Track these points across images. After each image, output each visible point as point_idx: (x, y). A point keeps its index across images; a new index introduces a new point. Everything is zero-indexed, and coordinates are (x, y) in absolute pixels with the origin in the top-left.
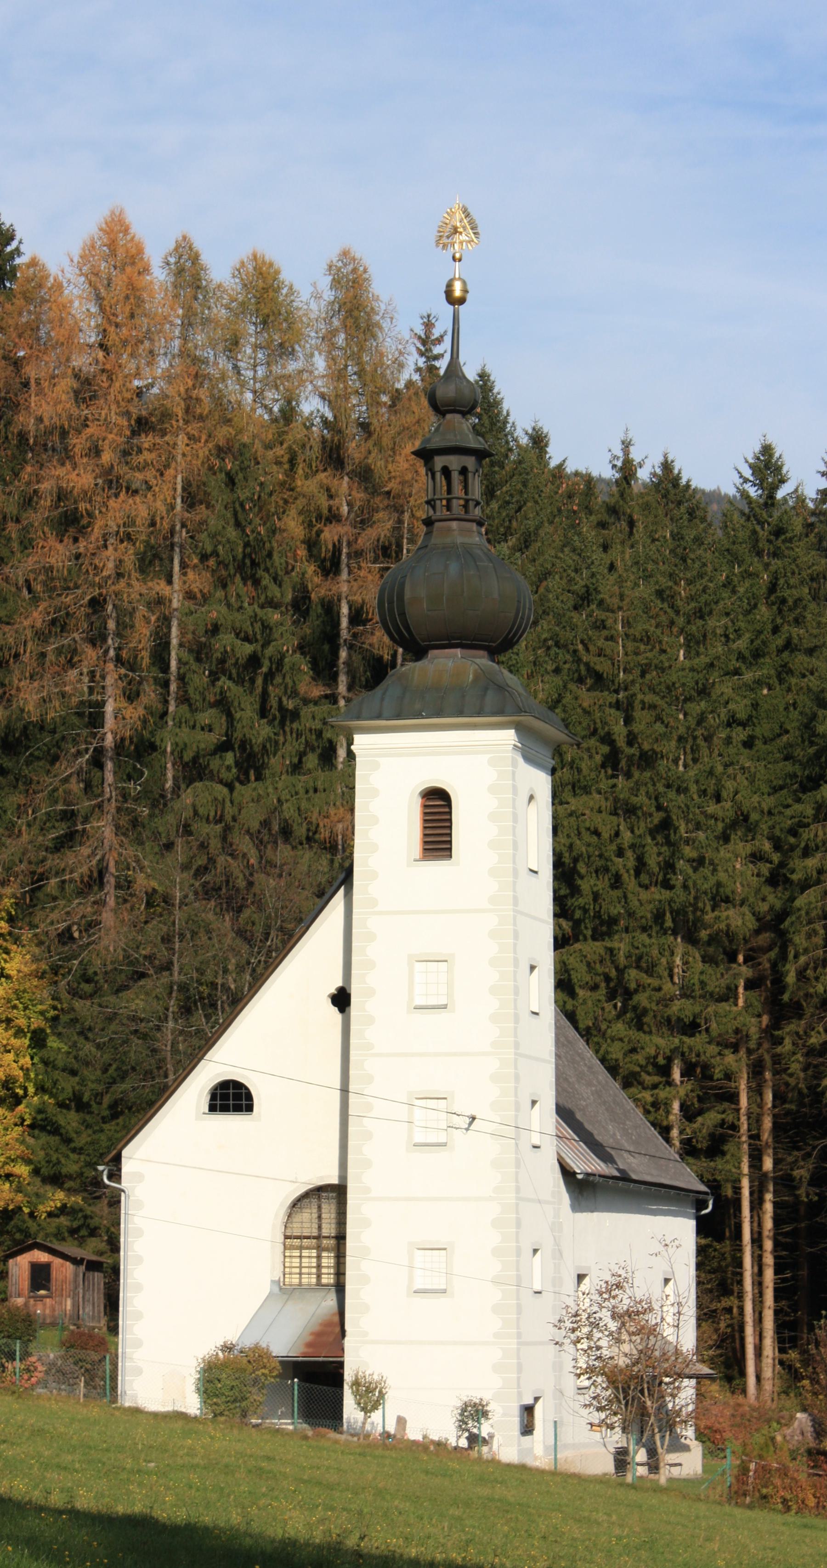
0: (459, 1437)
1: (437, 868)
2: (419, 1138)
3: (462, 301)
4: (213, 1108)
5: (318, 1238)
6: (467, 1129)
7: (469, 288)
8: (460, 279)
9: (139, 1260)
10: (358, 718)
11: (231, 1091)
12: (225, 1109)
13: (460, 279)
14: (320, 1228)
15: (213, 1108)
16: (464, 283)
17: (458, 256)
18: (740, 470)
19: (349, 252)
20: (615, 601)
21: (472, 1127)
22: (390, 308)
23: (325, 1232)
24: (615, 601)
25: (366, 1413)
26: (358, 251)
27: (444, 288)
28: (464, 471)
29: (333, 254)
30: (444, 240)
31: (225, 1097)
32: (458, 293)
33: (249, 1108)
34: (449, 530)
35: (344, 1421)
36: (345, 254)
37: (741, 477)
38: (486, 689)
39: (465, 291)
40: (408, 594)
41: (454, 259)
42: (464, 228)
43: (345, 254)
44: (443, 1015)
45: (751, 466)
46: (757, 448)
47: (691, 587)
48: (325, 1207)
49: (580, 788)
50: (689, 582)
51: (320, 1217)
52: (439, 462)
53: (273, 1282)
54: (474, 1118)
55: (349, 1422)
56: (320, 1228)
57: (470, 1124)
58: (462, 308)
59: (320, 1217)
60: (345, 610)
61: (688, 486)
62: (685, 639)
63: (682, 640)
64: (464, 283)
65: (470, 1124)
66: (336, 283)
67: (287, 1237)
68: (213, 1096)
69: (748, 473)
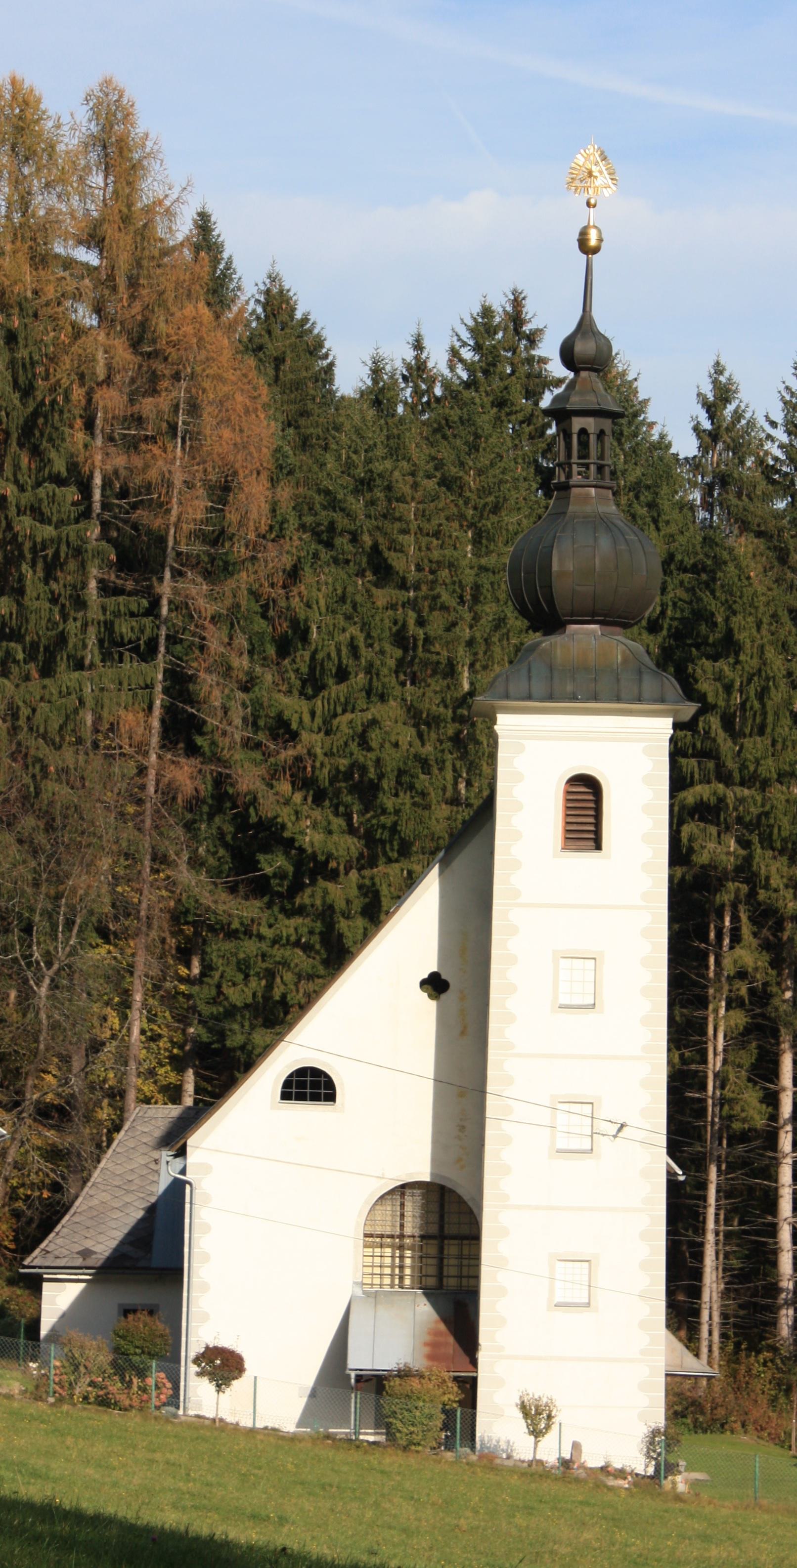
0: (647, 1466)
1: (586, 860)
2: (561, 1144)
3: (596, 250)
4: (286, 1096)
5: (402, 1236)
6: (615, 1136)
7: (604, 236)
8: (595, 227)
9: (206, 1258)
10: (507, 697)
11: (309, 1079)
12: (301, 1097)
13: (595, 227)
14: (402, 1226)
15: (286, 1096)
16: (599, 232)
17: (592, 201)
18: (460, 333)
19: (110, 80)
20: (407, 490)
21: (620, 1135)
22: (156, 147)
23: (408, 1230)
24: (407, 490)
25: (536, 1437)
26: (120, 81)
27: (577, 236)
28: (601, 434)
29: (93, 83)
30: (577, 183)
31: (301, 1085)
32: (593, 242)
33: (331, 1097)
34: (587, 497)
35: (477, 1439)
36: (107, 82)
37: (459, 340)
38: (640, 673)
39: (600, 240)
40: (555, 567)
41: (588, 204)
42: (601, 172)
43: (107, 82)
44: (591, 1015)
45: (472, 330)
46: (477, 309)
47: (482, 478)
48: (409, 1207)
49: (376, 695)
50: (480, 472)
51: (402, 1216)
52: (577, 423)
53: (355, 1283)
54: (622, 1126)
55: (482, 1441)
56: (402, 1226)
57: (620, 1130)
58: (595, 258)
59: (402, 1216)
60: (98, 481)
61: (305, 320)
62: (474, 534)
63: (470, 534)
64: (599, 232)
65: (620, 1130)
66: (96, 113)
67: (366, 1235)
68: (287, 1084)
69: (465, 335)
